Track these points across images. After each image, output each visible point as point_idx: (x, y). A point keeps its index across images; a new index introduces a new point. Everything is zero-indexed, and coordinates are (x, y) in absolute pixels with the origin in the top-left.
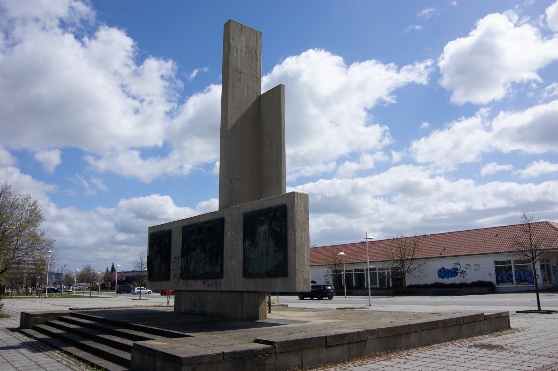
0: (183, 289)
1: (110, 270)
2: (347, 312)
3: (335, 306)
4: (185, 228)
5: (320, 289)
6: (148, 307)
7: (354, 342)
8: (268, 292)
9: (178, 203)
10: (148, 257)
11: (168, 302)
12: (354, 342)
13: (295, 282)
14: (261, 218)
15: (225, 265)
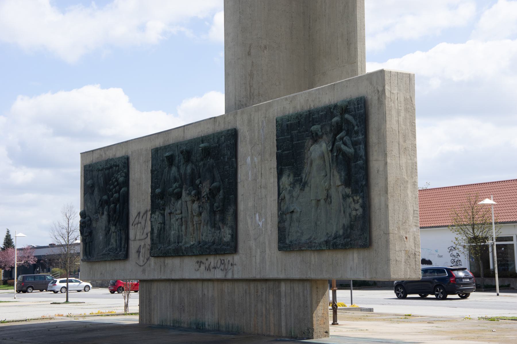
0: (156, 277)
2: (503, 326)
3: (476, 313)
4: (156, 152)
5: (441, 275)
6: (85, 316)
8: (330, 282)
9: (140, 103)
10: (83, 215)
11: (126, 306)
13: (388, 260)
14: (315, 128)
15: (241, 226)
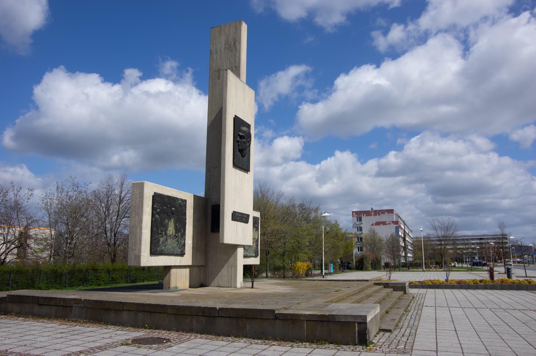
1: (450, 225)
7: (61, 306)
12: (61, 306)
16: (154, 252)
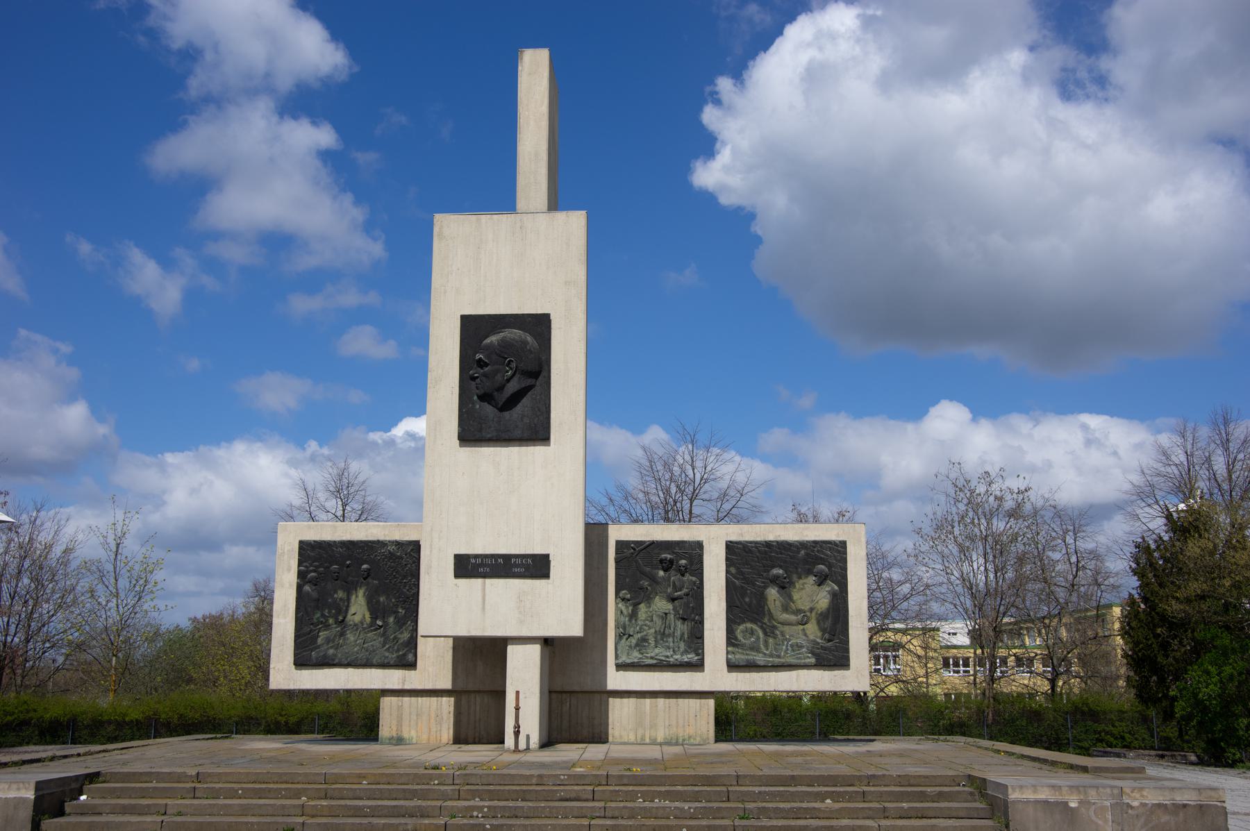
16: (301, 662)
